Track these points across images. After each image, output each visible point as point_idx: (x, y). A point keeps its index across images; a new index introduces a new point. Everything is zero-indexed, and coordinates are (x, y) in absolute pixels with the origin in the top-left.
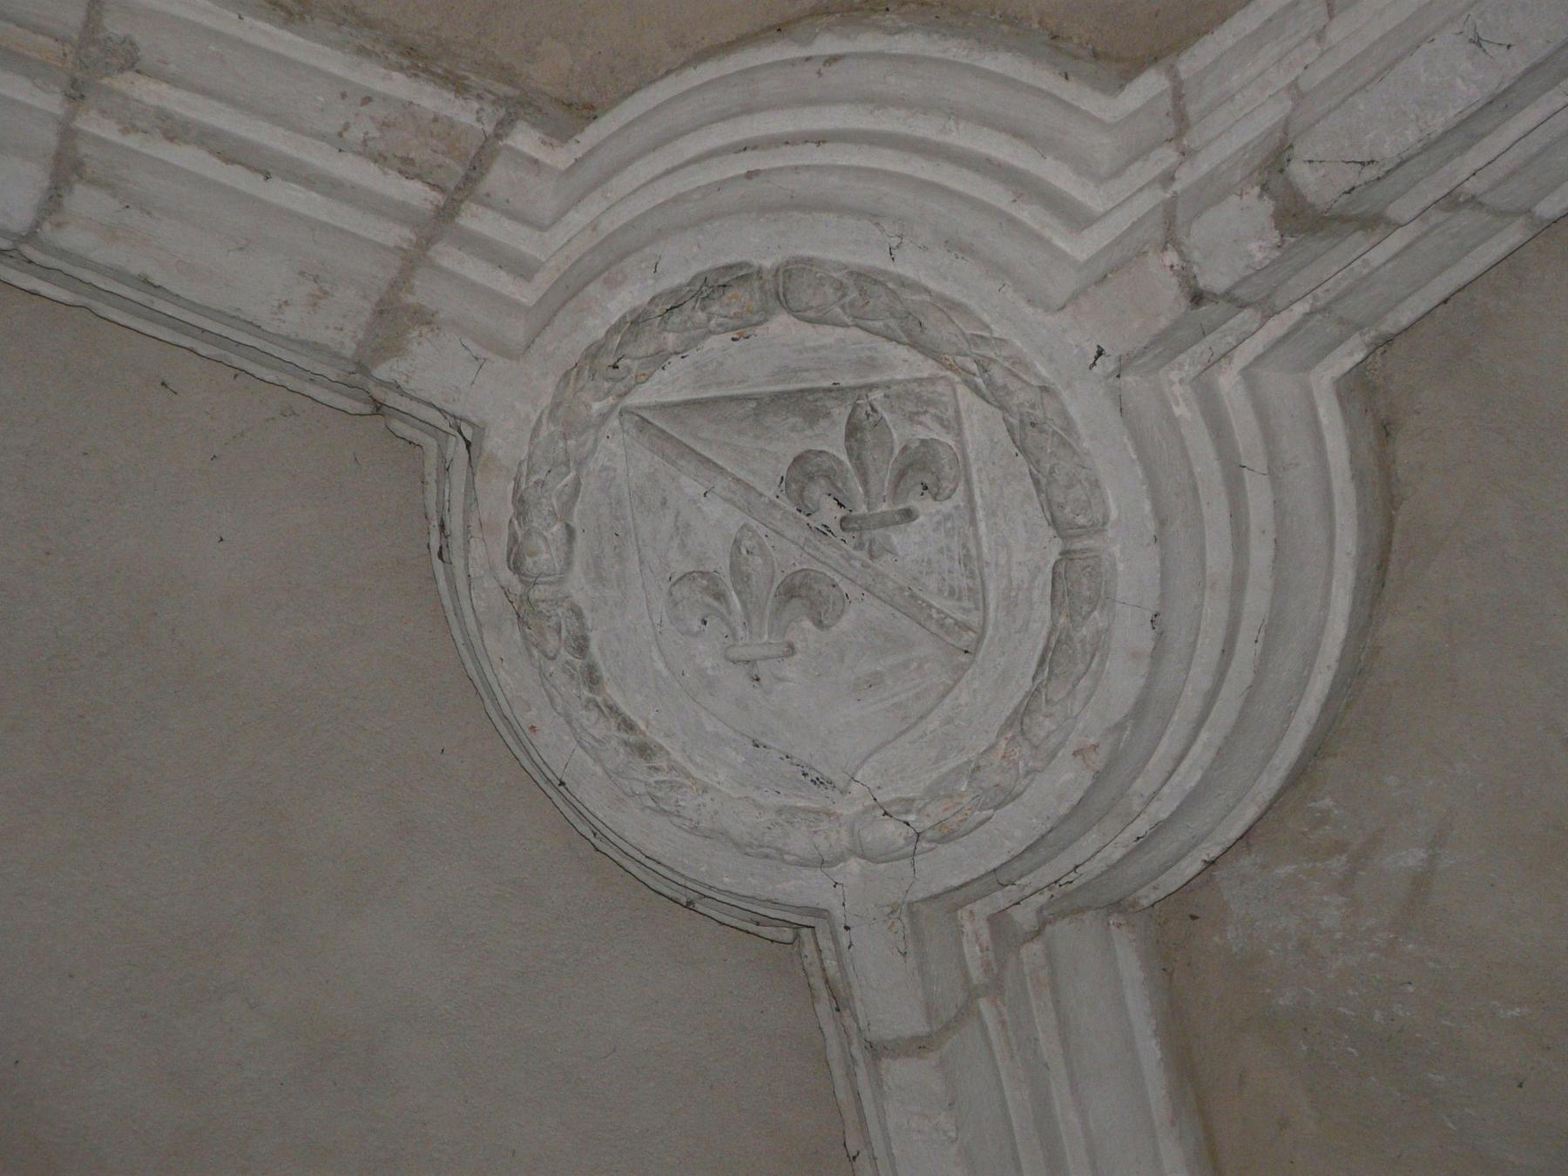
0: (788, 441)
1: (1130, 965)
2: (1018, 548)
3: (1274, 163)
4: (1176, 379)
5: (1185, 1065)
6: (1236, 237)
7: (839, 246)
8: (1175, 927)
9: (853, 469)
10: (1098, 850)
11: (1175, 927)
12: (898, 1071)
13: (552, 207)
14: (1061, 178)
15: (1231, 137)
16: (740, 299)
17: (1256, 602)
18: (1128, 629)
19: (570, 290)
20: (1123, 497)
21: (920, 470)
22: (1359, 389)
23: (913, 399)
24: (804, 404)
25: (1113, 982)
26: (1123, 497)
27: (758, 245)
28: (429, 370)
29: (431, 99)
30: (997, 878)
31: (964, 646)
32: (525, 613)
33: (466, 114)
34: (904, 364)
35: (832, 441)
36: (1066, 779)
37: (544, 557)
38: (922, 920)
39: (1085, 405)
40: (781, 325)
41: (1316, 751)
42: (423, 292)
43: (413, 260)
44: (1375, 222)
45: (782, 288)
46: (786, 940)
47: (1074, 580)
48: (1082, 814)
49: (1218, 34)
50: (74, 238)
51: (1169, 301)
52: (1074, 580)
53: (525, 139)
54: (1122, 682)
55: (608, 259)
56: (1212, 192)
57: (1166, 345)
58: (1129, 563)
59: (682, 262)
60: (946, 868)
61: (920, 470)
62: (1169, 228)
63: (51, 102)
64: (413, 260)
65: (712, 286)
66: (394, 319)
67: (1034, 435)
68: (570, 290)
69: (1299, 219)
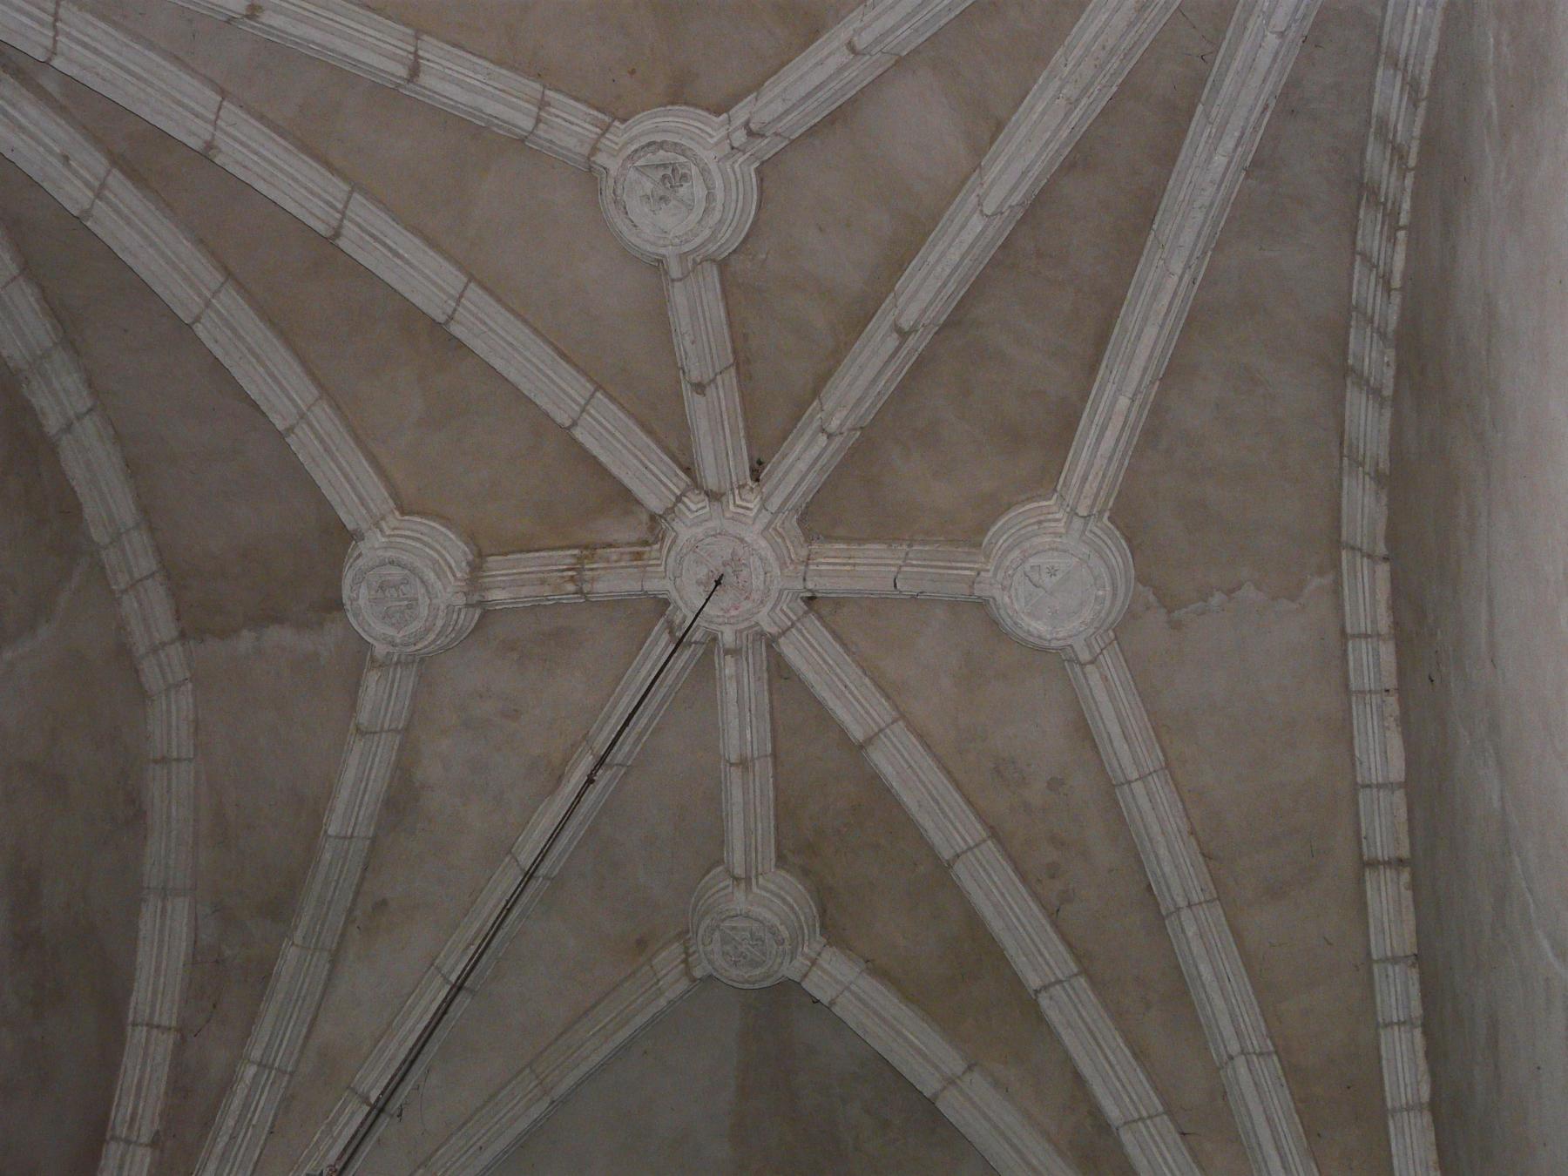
0: (661, 173)
1: (716, 272)
2: (700, 192)
3: (746, 125)
4: (728, 164)
5: (724, 291)
6: (740, 137)
7: (670, 138)
8: (723, 265)
9: (673, 177)
10: (712, 248)
11: (723, 265)
12: (677, 284)
13: (620, 135)
14: (708, 130)
15: (739, 121)
16: (652, 148)
17: (740, 205)
18: (719, 207)
19: (626, 144)
20: (719, 183)
21: (684, 177)
22: (758, 171)
23: (681, 164)
24: (665, 166)
25: (713, 274)
26: (719, 183)
27: (658, 138)
28: (601, 159)
29: (600, 116)
30: (694, 250)
31: (690, 208)
32: (615, 202)
33: (607, 119)
34: (682, 159)
35: (669, 172)
36: (707, 232)
37: (619, 192)
38: (682, 257)
39: (713, 167)
40: (661, 152)
41: (747, 236)
42: (599, 145)
43: (598, 141)
44: (763, 136)
45: (662, 145)
46: (658, 265)
47: (710, 197)
48: (708, 240)
49: (1071, 1049)
50: (540, 133)
51: (728, 148)
52: (710, 197)
53: (617, 123)
54: (717, 215)
55: (631, 141)
56: (736, 130)
57: (727, 157)
58: (720, 195)
59: (645, 140)
60: (686, 248)
61: (684, 177)
62: (728, 136)
63: (535, 109)
64: (598, 141)
65: (649, 144)
66: (595, 150)
67: (704, 171)
68: (626, 144)
69: (750, 133)
